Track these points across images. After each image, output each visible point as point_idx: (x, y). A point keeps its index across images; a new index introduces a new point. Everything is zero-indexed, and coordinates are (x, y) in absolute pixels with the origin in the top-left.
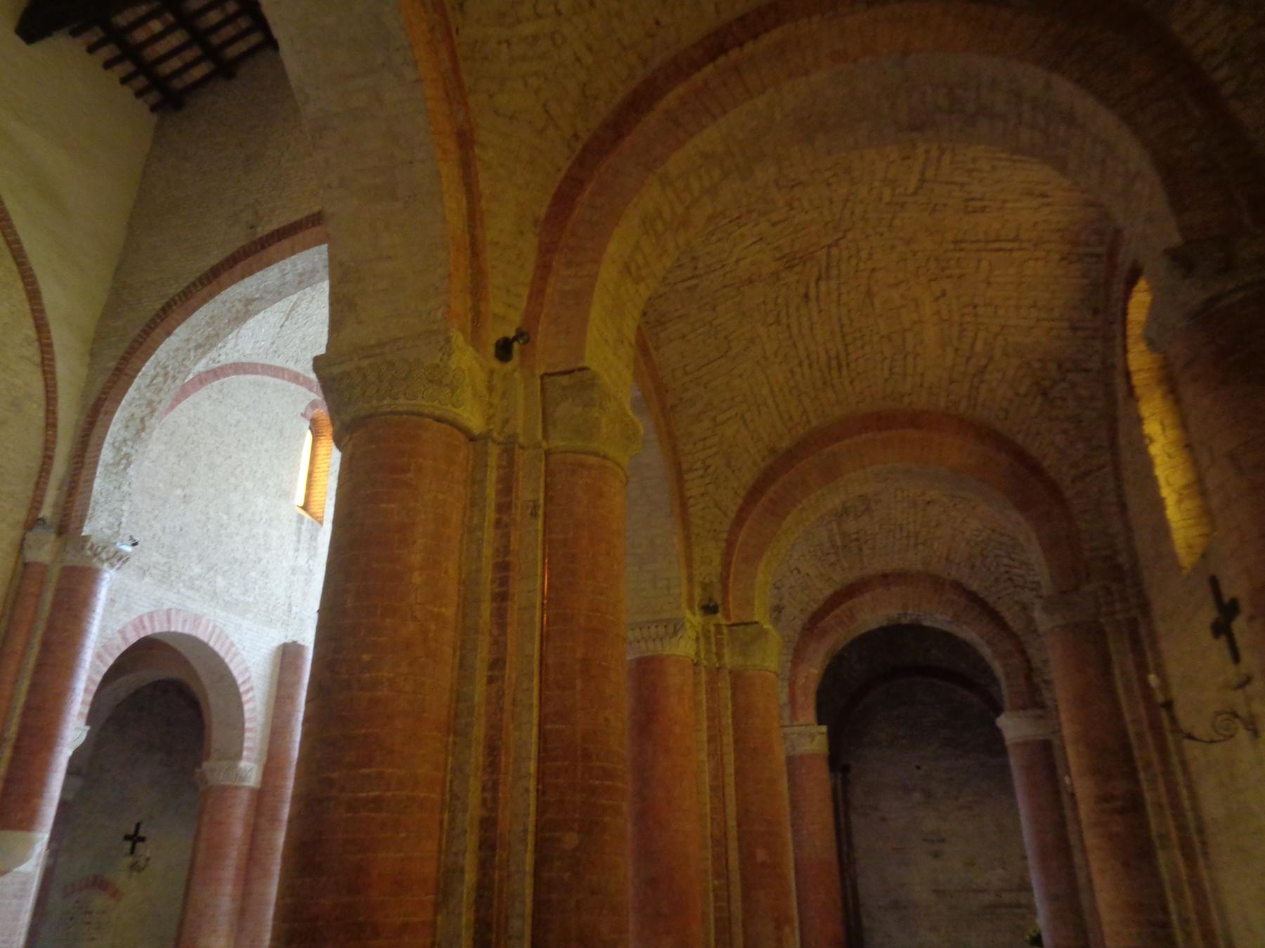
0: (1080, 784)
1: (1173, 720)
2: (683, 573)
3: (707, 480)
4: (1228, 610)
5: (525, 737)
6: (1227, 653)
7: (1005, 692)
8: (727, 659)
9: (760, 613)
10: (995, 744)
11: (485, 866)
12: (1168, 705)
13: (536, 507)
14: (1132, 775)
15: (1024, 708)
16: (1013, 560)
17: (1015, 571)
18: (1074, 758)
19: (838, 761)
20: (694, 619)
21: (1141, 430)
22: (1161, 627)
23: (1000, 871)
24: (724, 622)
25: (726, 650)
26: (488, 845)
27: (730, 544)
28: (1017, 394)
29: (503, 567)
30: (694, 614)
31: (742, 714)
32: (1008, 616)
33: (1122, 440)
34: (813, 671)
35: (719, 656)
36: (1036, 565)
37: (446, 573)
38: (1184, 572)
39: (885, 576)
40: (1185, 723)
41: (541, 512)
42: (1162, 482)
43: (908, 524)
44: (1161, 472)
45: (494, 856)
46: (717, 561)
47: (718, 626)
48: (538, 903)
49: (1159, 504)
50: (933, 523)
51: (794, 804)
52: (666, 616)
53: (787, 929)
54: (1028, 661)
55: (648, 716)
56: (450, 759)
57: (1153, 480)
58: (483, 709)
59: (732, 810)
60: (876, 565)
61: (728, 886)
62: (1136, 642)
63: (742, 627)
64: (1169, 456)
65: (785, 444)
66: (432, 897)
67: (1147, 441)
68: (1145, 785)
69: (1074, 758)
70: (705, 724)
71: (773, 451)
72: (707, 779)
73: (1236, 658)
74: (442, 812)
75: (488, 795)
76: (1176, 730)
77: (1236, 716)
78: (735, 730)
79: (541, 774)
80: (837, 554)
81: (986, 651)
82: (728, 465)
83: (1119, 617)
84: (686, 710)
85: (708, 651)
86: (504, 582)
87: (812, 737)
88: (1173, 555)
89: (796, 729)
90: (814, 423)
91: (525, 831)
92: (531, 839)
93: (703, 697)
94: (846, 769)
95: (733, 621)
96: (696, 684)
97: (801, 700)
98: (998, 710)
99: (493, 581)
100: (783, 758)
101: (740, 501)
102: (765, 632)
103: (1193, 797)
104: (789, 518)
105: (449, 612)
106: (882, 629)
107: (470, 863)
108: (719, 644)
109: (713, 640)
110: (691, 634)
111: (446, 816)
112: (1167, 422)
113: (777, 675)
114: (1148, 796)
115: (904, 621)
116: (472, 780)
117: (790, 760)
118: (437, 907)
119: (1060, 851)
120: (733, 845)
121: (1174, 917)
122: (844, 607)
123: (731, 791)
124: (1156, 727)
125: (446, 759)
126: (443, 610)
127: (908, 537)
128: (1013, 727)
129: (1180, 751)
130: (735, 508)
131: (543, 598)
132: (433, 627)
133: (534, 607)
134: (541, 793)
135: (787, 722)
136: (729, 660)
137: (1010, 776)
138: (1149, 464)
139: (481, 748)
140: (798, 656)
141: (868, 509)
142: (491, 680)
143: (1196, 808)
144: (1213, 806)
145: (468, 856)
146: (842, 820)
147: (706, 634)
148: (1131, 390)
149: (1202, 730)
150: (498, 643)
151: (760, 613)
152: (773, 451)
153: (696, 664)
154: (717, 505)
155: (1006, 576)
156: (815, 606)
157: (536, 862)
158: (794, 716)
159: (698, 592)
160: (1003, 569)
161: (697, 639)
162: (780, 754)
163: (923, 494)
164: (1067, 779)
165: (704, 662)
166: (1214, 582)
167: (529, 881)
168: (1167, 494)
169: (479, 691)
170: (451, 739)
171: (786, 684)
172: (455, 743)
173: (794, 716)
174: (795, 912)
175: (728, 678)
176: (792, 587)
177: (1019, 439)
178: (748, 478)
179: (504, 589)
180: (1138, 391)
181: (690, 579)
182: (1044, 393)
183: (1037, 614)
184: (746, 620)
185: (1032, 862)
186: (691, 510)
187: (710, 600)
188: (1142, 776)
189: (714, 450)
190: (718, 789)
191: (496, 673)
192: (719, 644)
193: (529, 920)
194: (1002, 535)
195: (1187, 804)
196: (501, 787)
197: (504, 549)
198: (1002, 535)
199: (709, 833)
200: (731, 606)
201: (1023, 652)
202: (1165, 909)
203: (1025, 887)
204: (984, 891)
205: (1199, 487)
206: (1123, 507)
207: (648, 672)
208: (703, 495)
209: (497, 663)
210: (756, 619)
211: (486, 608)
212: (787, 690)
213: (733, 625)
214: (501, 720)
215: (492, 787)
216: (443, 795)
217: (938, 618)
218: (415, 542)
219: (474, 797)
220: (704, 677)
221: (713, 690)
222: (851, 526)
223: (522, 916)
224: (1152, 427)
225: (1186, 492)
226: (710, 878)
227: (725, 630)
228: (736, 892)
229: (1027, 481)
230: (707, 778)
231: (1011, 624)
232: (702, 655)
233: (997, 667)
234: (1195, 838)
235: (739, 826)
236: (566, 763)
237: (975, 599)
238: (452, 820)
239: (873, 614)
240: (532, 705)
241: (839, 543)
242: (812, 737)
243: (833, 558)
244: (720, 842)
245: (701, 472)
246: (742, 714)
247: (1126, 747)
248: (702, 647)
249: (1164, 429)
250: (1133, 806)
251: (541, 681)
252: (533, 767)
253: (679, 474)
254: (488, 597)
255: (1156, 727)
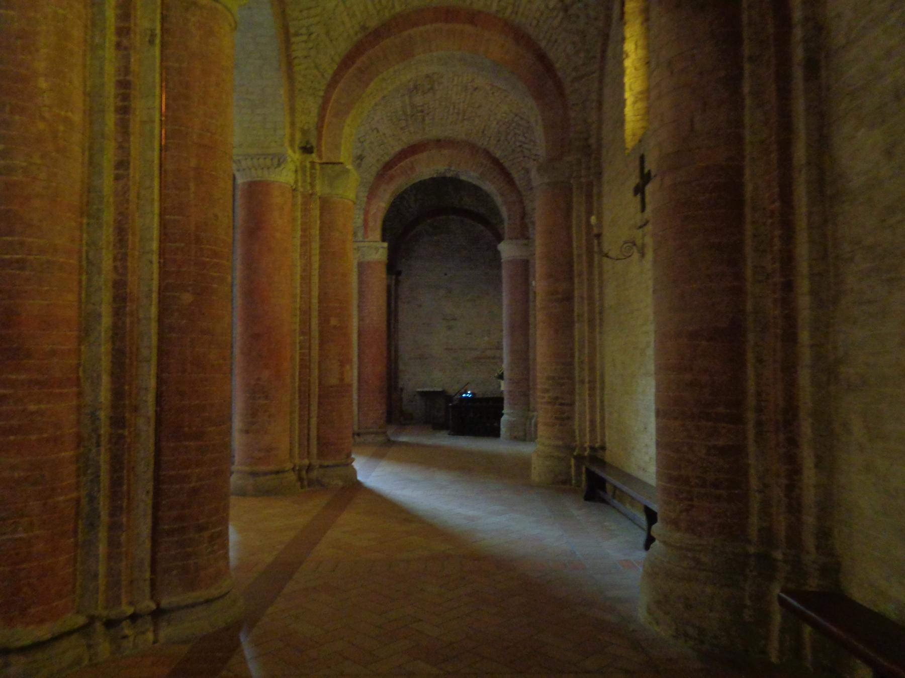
0: (539, 284)
1: (599, 244)
2: (288, 119)
3: (311, 45)
4: (646, 178)
5: (148, 223)
6: (639, 207)
7: (506, 230)
8: (318, 188)
9: (345, 156)
10: (495, 260)
11: (118, 313)
12: (599, 236)
13: (153, 35)
14: (571, 279)
15: (517, 238)
16: (526, 137)
17: (526, 146)
18: (539, 268)
19: (393, 267)
20: (294, 156)
21: (622, 48)
22: (606, 188)
23: (486, 338)
24: (317, 160)
25: (318, 182)
26: (121, 297)
27: (326, 100)
28: (547, 7)
29: (124, 85)
30: (294, 152)
31: (326, 228)
32: (516, 176)
33: (610, 53)
34: (382, 205)
35: (312, 185)
36: (540, 143)
37: (71, 82)
38: (627, 152)
39: (439, 141)
40: (606, 247)
41: (158, 41)
42: (627, 87)
43: (459, 103)
44: (627, 80)
45: (125, 307)
46: (315, 110)
47: (313, 163)
48: (161, 339)
49: (622, 103)
50: (477, 105)
51: (361, 293)
52: (271, 151)
53: (348, 367)
54: (524, 208)
55: (256, 226)
56: (85, 236)
57: (622, 85)
58: (111, 200)
59: (315, 292)
60: (435, 132)
61: (310, 340)
62: (589, 196)
63: (330, 166)
64: (636, 69)
65: (373, 23)
66: (75, 333)
67: (624, 56)
68: (576, 286)
69: (539, 268)
70: (299, 234)
71: (364, 28)
72: (299, 272)
73: (643, 209)
74: (80, 274)
75: (118, 264)
76: (601, 251)
77: (635, 245)
78: (321, 239)
79: (162, 252)
80: (407, 120)
81: (499, 200)
82: (327, 34)
83: (583, 180)
84: (286, 226)
85: (304, 181)
86: (126, 97)
87: (377, 249)
88: (623, 140)
89: (366, 244)
90: (398, 9)
91: (151, 291)
92: (155, 296)
93: (299, 214)
94: (399, 273)
95: (324, 160)
96: (294, 204)
97: (371, 224)
98: (499, 238)
99: (116, 97)
100: (355, 263)
101: (335, 67)
102: (348, 171)
103: (601, 293)
104: (372, 85)
105: (77, 118)
106: (433, 179)
107: (106, 311)
108: (313, 177)
109: (308, 174)
110: (291, 166)
111: (84, 277)
112: (640, 43)
113: (355, 203)
114: (576, 293)
115: (449, 175)
116: (104, 251)
117: (360, 265)
118: (80, 341)
119: (522, 326)
120: (315, 314)
121: (576, 359)
122: (407, 160)
123: (315, 279)
124: (590, 252)
125: (81, 236)
126: (70, 114)
127: (458, 114)
128: (507, 250)
129: (601, 266)
130: (331, 72)
131: (161, 115)
132: (61, 128)
133: (153, 122)
134: (162, 266)
135: (361, 239)
136: (320, 189)
137: (501, 282)
138: (621, 73)
139: (111, 230)
140: (372, 194)
141: (432, 88)
142: (117, 178)
143: (602, 299)
144: (611, 296)
145: (103, 306)
146: (393, 305)
147: (303, 168)
148: (623, 13)
149: (612, 254)
150: (123, 148)
151: (345, 156)
152: (364, 28)
153: (294, 190)
154: (317, 67)
155: (519, 149)
156: (387, 158)
157: (159, 312)
158: (365, 235)
159: (298, 135)
160: (518, 144)
161: (296, 171)
162: (353, 260)
163: (473, 81)
164: (534, 283)
165: (301, 189)
166: (642, 159)
167: (154, 327)
168: (629, 96)
169: (107, 183)
170: (85, 221)
171: (362, 212)
172: (88, 224)
173: (365, 235)
174: (355, 359)
175: (318, 202)
176: (372, 143)
177: (543, 44)
178: (343, 47)
179: (126, 103)
180: (627, 17)
181: (293, 124)
182: (566, 10)
183: (533, 174)
184: (334, 160)
185: (505, 333)
186: (297, 68)
187: (308, 142)
188: (576, 281)
189: (317, 19)
190: (306, 279)
191: (121, 172)
192: (313, 177)
193: (155, 351)
194: (522, 119)
195: (597, 297)
196: (129, 259)
197: (125, 69)
198: (522, 119)
199: (298, 306)
200: (323, 148)
201: (521, 202)
202: (572, 356)
203: (499, 347)
204: (476, 349)
205: (646, 94)
206: (600, 104)
207: (257, 192)
208: (306, 57)
209: (122, 164)
210: (341, 160)
211: (111, 119)
212: (362, 217)
213: (323, 163)
214: (127, 209)
215: (121, 259)
216: (80, 261)
217: (470, 175)
218: (37, 50)
219: (107, 262)
220: (300, 200)
221: (306, 210)
222: (418, 100)
223: (149, 347)
224: (629, 46)
225: (640, 96)
226: (298, 334)
227: (318, 167)
228: (315, 343)
229: (542, 74)
230: (299, 269)
231: (517, 182)
232: (300, 184)
233: (504, 211)
234: (597, 316)
235: (319, 303)
236: (183, 245)
237: (496, 162)
238: (89, 280)
239: (427, 168)
240: (153, 199)
241: (409, 112)
242: (377, 249)
243: (403, 124)
244: (306, 313)
245: (304, 38)
246: (326, 228)
247: (570, 264)
248: (299, 177)
249: (636, 48)
250: (568, 298)
251: (161, 182)
252: (155, 245)
253: (287, 37)
254: (112, 109)
255: (590, 252)
